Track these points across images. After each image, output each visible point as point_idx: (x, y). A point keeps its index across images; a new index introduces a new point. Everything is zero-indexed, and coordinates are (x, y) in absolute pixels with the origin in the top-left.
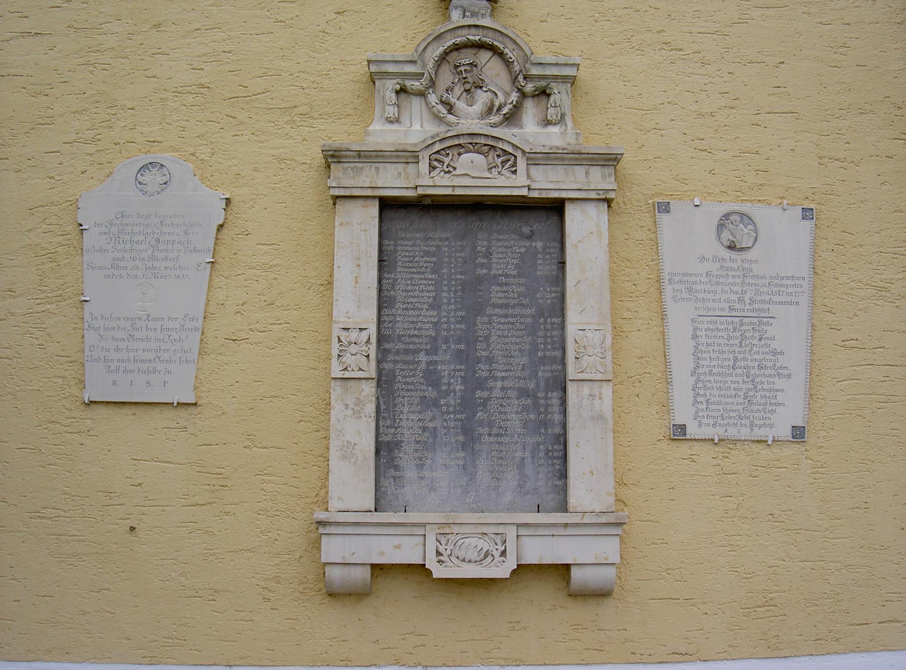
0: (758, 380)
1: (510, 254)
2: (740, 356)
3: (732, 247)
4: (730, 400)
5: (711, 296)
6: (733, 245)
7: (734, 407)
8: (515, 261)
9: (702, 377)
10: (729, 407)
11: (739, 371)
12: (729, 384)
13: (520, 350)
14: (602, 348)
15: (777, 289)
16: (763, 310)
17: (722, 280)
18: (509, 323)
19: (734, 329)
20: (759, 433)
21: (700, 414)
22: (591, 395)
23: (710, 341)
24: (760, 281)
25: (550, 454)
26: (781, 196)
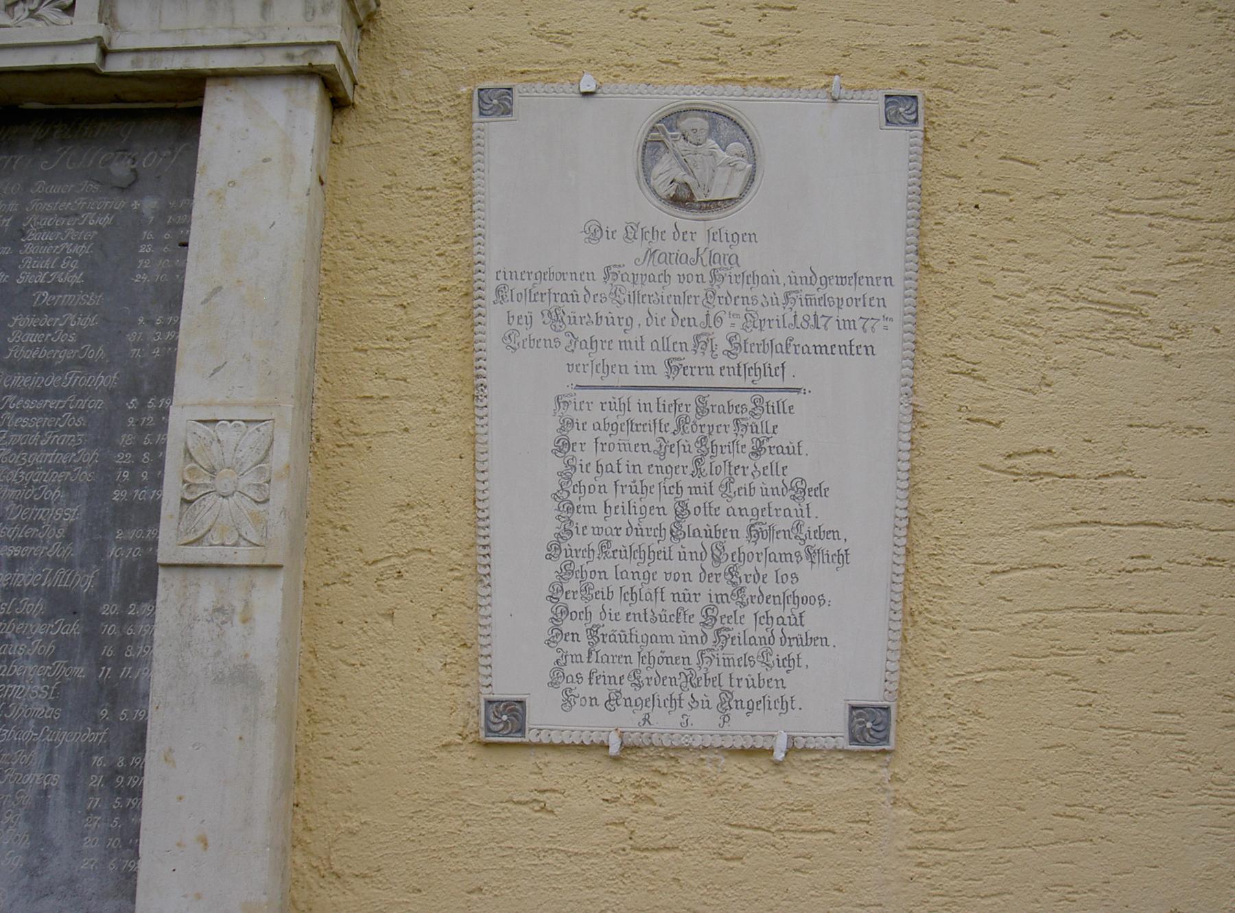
0: (747, 568)
1: (71, 232)
2: (694, 501)
3: (681, 200)
4: (661, 629)
5: (616, 333)
6: (684, 194)
7: (673, 650)
8: (80, 250)
9: (579, 562)
10: (656, 649)
11: (692, 544)
12: (660, 581)
13: (67, 486)
14: (261, 471)
15: (811, 311)
16: (767, 370)
17: (650, 288)
18: (46, 412)
19: (681, 425)
20: (746, 727)
21: (570, 669)
22: (219, 610)
23: (607, 458)
24: (761, 290)
25: (120, 780)
26: (829, 69)
